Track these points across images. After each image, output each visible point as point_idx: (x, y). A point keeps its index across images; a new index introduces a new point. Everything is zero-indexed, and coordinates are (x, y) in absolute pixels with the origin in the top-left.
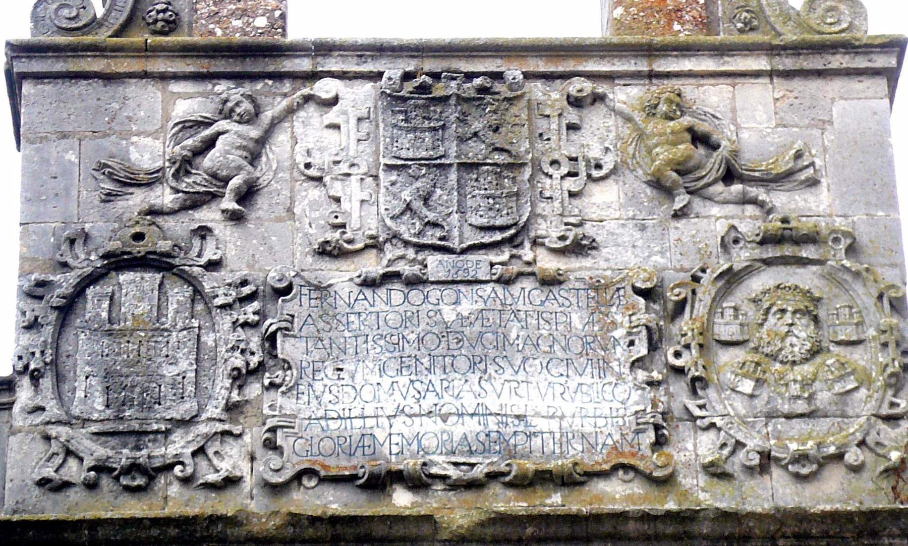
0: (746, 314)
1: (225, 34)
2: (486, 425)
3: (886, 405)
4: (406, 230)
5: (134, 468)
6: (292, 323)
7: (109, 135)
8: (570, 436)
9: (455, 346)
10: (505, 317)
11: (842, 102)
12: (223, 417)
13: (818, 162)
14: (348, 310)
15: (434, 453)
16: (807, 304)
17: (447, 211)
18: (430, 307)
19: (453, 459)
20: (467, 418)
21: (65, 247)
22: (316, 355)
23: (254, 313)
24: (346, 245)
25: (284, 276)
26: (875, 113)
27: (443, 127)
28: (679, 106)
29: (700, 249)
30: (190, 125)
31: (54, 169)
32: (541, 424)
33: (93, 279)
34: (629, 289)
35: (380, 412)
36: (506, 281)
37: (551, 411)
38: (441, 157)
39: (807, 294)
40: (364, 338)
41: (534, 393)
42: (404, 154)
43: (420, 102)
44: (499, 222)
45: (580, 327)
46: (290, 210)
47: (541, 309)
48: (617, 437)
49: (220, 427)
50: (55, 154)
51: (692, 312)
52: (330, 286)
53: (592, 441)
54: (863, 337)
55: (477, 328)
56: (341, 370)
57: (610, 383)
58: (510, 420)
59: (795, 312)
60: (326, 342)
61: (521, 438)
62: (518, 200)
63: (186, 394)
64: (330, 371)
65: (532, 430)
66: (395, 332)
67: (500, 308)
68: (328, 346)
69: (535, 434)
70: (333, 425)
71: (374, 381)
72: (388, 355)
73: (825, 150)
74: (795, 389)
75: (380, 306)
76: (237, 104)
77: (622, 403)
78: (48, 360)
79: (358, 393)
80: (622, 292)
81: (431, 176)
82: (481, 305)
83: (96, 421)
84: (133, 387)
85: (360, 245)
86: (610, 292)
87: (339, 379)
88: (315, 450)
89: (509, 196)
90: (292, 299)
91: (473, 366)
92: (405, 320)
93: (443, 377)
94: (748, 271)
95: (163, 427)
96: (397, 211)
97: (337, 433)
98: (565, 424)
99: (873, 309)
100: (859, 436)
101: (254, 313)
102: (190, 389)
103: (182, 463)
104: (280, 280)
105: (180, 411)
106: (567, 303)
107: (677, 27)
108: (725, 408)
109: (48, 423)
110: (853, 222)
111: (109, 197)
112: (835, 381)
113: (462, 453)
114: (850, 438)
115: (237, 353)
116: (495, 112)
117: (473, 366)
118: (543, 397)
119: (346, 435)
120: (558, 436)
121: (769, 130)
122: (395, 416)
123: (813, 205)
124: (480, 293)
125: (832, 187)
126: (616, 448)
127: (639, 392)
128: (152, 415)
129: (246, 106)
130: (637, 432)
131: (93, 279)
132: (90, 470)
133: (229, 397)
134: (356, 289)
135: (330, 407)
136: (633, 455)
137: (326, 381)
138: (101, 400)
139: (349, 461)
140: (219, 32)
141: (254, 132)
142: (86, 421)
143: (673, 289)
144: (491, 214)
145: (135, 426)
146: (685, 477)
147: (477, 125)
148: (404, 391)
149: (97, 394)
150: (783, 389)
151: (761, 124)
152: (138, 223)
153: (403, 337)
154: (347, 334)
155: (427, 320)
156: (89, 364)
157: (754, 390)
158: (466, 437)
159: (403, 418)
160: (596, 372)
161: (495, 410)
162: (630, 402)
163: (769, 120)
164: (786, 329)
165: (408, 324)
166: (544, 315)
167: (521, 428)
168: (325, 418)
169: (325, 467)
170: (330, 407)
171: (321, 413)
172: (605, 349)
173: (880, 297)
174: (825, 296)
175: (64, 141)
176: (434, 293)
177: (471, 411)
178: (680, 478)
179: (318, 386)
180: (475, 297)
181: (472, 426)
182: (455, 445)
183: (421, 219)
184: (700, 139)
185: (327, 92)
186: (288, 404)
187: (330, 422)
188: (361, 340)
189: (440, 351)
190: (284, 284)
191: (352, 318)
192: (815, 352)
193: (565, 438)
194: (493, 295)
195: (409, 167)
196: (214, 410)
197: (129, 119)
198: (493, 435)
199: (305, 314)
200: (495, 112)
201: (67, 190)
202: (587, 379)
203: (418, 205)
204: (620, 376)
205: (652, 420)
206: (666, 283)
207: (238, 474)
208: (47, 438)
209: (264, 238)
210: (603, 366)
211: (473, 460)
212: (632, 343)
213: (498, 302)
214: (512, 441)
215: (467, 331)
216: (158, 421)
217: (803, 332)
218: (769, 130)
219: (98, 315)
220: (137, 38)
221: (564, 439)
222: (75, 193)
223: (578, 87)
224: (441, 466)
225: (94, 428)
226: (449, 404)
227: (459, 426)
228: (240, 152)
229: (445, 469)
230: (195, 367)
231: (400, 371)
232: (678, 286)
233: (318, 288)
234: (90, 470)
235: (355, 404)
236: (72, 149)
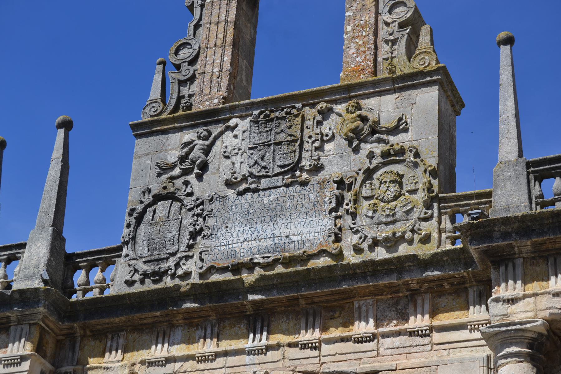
0: (375, 185)
1: (203, 108)
2: (274, 241)
3: (423, 213)
4: (254, 171)
5: (154, 273)
6: (212, 212)
7: (161, 152)
8: (305, 241)
9: (266, 213)
10: (285, 199)
11: (420, 95)
12: (186, 250)
13: (409, 121)
14: (232, 204)
15: (256, 254)
16: (395, 178)
17: (270, 161)
18: (260, 199)
19: (263, 256)
20: (268, 239)
21: (142, 195)
22: (219, 223)
23: (200, 210)
24: (233, 180)
25: (210, 195)
26: (433, 97)
27: (271, 130)
28: (359, 108)
29: (361, 162)
30: (186, 144)
31: (142, 167)
32: (295, 238)
33: (149, 205)
34: (332, 181)
35: (239, 241)
36: (287, 186)
37: (299, 232)
38: (269, 142)
39: (398, 174)
40: (236, 214)
41: (293, 227)
42: (256, 142)
43: (263, 122)
44: (287, 162)
45: (313, 199)
46: (218, 169)
47: (300, 194)
48: (321, 240)
49: (184, 254)
50: (143, 162)
51: (354, 187)
52: (227, 196)
53: (312, 242)
54: (417, 187)
55: (275, 205)
56: (227, 227)
57: (321, 219)
58: (283, 238)
59: (390, 182)
60: (223, 217)
61: (287, 244)
62: (295, 153)
63: (174, 243)
64: (223, 228)
65: (291, 241)
66: (246, 210)
67: (284, 195)
68: (224, 219)
69: (292, 242)
70: (222, 248)
71: (237, 230)
72: (243, 219)
73: (412, 115)
74: (387, 212)
75: (243, 201)
76: (201, 133)
77: (325, 226)
78: (131, 237)
79: (232, 235)
80: (329, 183)
81: (265, 149)
82: (278, 196)
83: (144, 257)
84: (157, 243)
85: (239, 179)
86: (325, 184)
87: (226, 230)
88: (215, 258)
89: (291, 152)
90: (213, 203)
91: (271, 220)
92: (251, 205)
93: (261, 225)
94: (377, 169)
95: (166, 256)
96: (252, 165)
97: (223, 251)
98: (303, 237)
99: (422, 175)
100: (411, 227)
101: (200, 210)
102: (176, 241)
103: (171, 269)
104: (209, 197)
105: (172, 250)
106: (309, 190)
107: (362, 76)
108: (362, 223)
109: (130, 260)
110: (420, 142)
111: (159, 175)
112: (403, 207)
113: (266, 253)
114: (407, 228)
115: (192, 226)
116: (290, 121)
117: (271, 220)
118: (296, 228)
119: (226, 251)
120: (300, 242)
121: (392, 111)
122: (243, 242)
123: (405, 138)
124: (278, 191)
125: (413, 129)
126: (321, 244)
127: (331, 221)
128: (162, 252)
129: (205, 133)
130: (329, 236)
131: (149, 205)
132: (141, 275)
133: (189, 242)
134: (236, 196)
135: (222, 241)
136: (326, 246)
137: (222, 232)
138: (146, 249)
139: (226, 261)
140: (201, 107)
141: (207, 143)
142: (141, 257)
143: (347, 179)
144: (285, 160)
145: (157, 257)
146: (346, 252)
147: (283, 127)
148: (247, 232)
149: (145, 247)
150: (383, 213)
151: (389, 109)
152: (165, 182)
153: (249, 212)
154: (231, 213)
155: (258, 204)
156: (144, 237)
157: (373, 214)
158: (267, 247)
159: (246, 242)
160: (317, 215)
161: (278, 235)
162: (328, 225)
163: (392, 107)
164: (386, 188)
165: (251, 207)
166: (300, 196)
167: (287, 241)
168: (220, 246)
169: (217, 264)
170: (222, 241)
171: (219, 244)
172: (321, 206)
173: (425, 171)
174: (405, 173)
175: (146, 157)
176: (262, 193)
177: (269, 236)
178: (344, 253)
179: (219, 234)
180: (276, 193)
181: (270, 242)
182: (263, 250)
183: (260, 166)
184: (364, 119)
185: (233, 123)
186: (208, 242)
187: (221, 247)
188: (235, 215)
189: (261, 215)
190: (210, 197)
191: (233, 207)
192: (396, 198)
193: (303, 242)
194: (283, 191)
195: (257, 147)
196: (183, 248)
197: (169, 145)
198: (277, 245)
199: (217, 208)
200: (290, 121)
201: (146, 174)
202: (313, 219)
203: (259, 161)
204: (325, 216)
205: (333, 231)
206: (344, 178)
207: (189, 270)
208: (129, 265)
209: (208, 181)
210: (320, 213)
211: (269, 255)
212: (331, 202)
213: (284, 193)
214: (283, 246)
215: (271, 206)
216: (164, 254)
217: (393, 189)
218: (392, 111)
219: (149, 218)
220: (180, 113)
221: (302, 243)
222: (148, 175)
223: (321, 106)
224: (258, 259)
225: (144, 260)
226: (262, 234)
227: (265, 243)
228: (201, 151)
229: (259, 260)
230: (178, 233)
231: (246, 225)
232: (350, 177)
233: (223, 197)
234: (141, 275)
235: (230, 239)
236: (149, 159)
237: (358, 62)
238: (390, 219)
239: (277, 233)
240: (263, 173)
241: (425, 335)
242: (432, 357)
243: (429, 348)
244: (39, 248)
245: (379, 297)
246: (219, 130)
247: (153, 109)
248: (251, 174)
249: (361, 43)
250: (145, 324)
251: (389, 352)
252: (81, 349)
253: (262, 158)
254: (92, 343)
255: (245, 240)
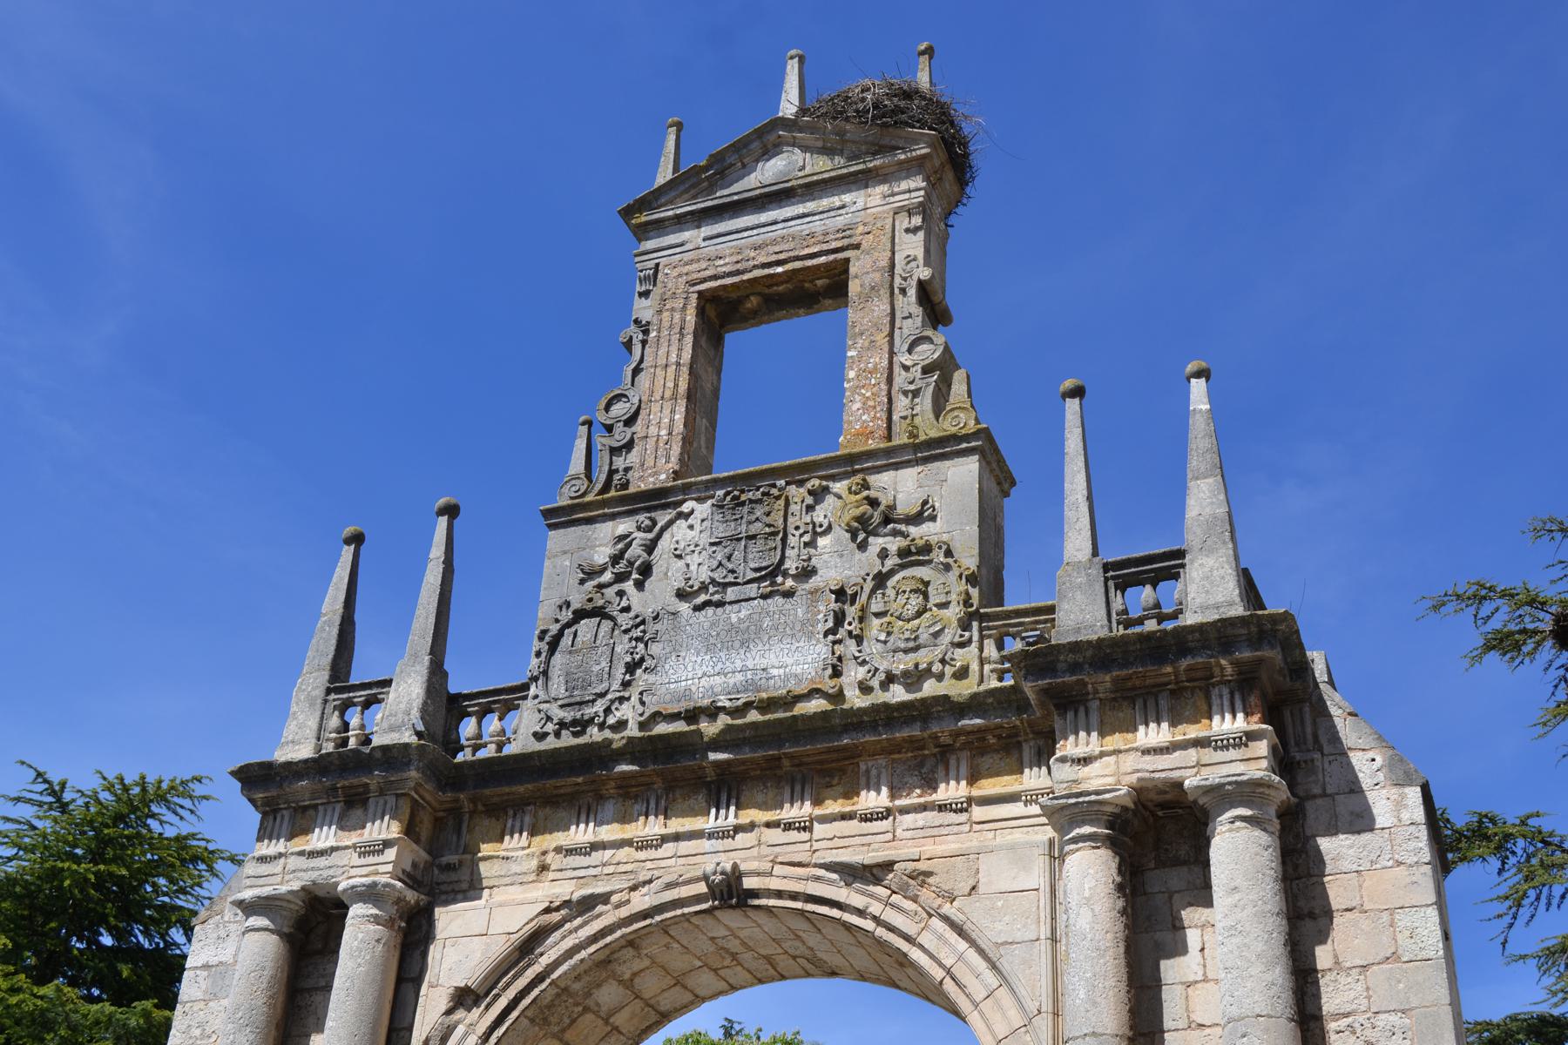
22: (668, 650)
32: (775, 672)
46: (666, 574)
49: (618, 694)
70: (672, 686)
111: (582, 582)
141: (650, 536)
142: (556, 700)
181: (739, 677)
184: (874, 503)
193: (787, 677)
196: (616, 686)
203: (725, 562)
210: (810, 635)
224: (724, 702)
225: (560, 703)
237: (864, 422)
238: (911, 644)
239: (750, 664)
240: (730, 579)
241: (961, 811)
242: (972, 841)
243: (966, 828)
244: (410, 686)
245: (896, 756)
246: (668, 518)
247: (574, 489)
248: (713, 581)
249: (868, 394)
250: (562, 795)
251: (909, 834)
252: (470, 831)
253: (729, 558)
254: (486, 822)
255: (704, 674)
